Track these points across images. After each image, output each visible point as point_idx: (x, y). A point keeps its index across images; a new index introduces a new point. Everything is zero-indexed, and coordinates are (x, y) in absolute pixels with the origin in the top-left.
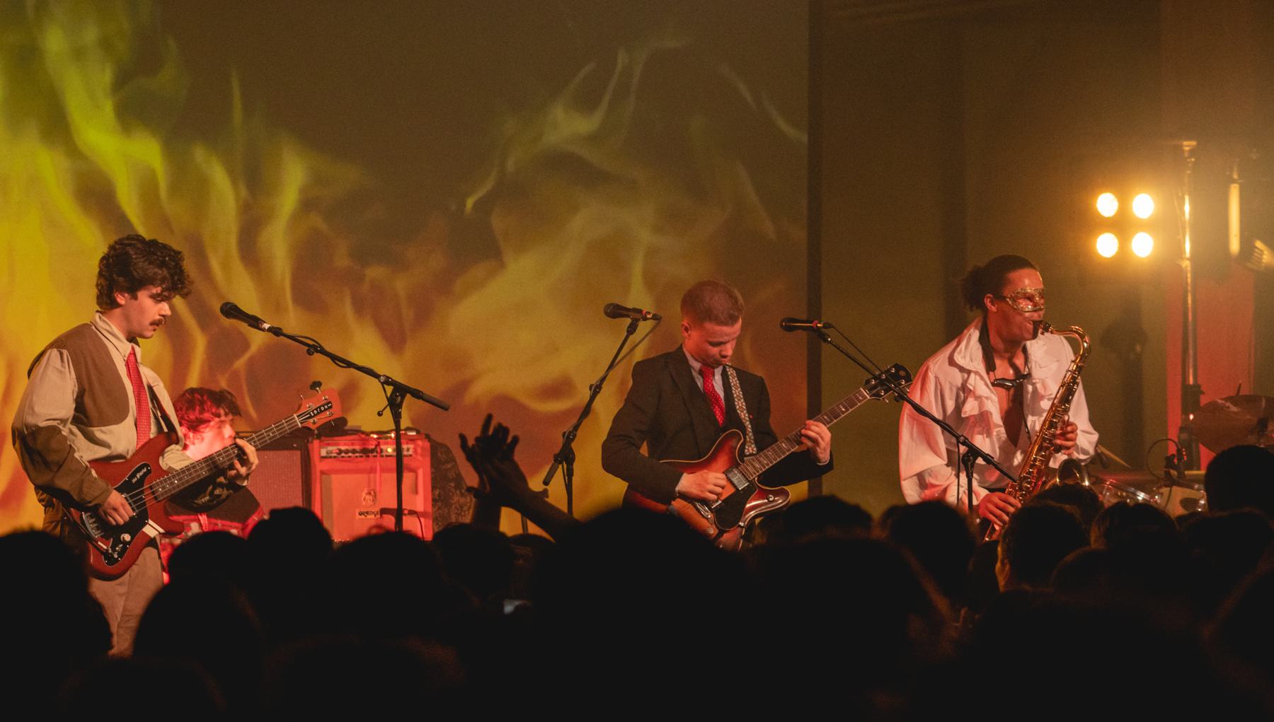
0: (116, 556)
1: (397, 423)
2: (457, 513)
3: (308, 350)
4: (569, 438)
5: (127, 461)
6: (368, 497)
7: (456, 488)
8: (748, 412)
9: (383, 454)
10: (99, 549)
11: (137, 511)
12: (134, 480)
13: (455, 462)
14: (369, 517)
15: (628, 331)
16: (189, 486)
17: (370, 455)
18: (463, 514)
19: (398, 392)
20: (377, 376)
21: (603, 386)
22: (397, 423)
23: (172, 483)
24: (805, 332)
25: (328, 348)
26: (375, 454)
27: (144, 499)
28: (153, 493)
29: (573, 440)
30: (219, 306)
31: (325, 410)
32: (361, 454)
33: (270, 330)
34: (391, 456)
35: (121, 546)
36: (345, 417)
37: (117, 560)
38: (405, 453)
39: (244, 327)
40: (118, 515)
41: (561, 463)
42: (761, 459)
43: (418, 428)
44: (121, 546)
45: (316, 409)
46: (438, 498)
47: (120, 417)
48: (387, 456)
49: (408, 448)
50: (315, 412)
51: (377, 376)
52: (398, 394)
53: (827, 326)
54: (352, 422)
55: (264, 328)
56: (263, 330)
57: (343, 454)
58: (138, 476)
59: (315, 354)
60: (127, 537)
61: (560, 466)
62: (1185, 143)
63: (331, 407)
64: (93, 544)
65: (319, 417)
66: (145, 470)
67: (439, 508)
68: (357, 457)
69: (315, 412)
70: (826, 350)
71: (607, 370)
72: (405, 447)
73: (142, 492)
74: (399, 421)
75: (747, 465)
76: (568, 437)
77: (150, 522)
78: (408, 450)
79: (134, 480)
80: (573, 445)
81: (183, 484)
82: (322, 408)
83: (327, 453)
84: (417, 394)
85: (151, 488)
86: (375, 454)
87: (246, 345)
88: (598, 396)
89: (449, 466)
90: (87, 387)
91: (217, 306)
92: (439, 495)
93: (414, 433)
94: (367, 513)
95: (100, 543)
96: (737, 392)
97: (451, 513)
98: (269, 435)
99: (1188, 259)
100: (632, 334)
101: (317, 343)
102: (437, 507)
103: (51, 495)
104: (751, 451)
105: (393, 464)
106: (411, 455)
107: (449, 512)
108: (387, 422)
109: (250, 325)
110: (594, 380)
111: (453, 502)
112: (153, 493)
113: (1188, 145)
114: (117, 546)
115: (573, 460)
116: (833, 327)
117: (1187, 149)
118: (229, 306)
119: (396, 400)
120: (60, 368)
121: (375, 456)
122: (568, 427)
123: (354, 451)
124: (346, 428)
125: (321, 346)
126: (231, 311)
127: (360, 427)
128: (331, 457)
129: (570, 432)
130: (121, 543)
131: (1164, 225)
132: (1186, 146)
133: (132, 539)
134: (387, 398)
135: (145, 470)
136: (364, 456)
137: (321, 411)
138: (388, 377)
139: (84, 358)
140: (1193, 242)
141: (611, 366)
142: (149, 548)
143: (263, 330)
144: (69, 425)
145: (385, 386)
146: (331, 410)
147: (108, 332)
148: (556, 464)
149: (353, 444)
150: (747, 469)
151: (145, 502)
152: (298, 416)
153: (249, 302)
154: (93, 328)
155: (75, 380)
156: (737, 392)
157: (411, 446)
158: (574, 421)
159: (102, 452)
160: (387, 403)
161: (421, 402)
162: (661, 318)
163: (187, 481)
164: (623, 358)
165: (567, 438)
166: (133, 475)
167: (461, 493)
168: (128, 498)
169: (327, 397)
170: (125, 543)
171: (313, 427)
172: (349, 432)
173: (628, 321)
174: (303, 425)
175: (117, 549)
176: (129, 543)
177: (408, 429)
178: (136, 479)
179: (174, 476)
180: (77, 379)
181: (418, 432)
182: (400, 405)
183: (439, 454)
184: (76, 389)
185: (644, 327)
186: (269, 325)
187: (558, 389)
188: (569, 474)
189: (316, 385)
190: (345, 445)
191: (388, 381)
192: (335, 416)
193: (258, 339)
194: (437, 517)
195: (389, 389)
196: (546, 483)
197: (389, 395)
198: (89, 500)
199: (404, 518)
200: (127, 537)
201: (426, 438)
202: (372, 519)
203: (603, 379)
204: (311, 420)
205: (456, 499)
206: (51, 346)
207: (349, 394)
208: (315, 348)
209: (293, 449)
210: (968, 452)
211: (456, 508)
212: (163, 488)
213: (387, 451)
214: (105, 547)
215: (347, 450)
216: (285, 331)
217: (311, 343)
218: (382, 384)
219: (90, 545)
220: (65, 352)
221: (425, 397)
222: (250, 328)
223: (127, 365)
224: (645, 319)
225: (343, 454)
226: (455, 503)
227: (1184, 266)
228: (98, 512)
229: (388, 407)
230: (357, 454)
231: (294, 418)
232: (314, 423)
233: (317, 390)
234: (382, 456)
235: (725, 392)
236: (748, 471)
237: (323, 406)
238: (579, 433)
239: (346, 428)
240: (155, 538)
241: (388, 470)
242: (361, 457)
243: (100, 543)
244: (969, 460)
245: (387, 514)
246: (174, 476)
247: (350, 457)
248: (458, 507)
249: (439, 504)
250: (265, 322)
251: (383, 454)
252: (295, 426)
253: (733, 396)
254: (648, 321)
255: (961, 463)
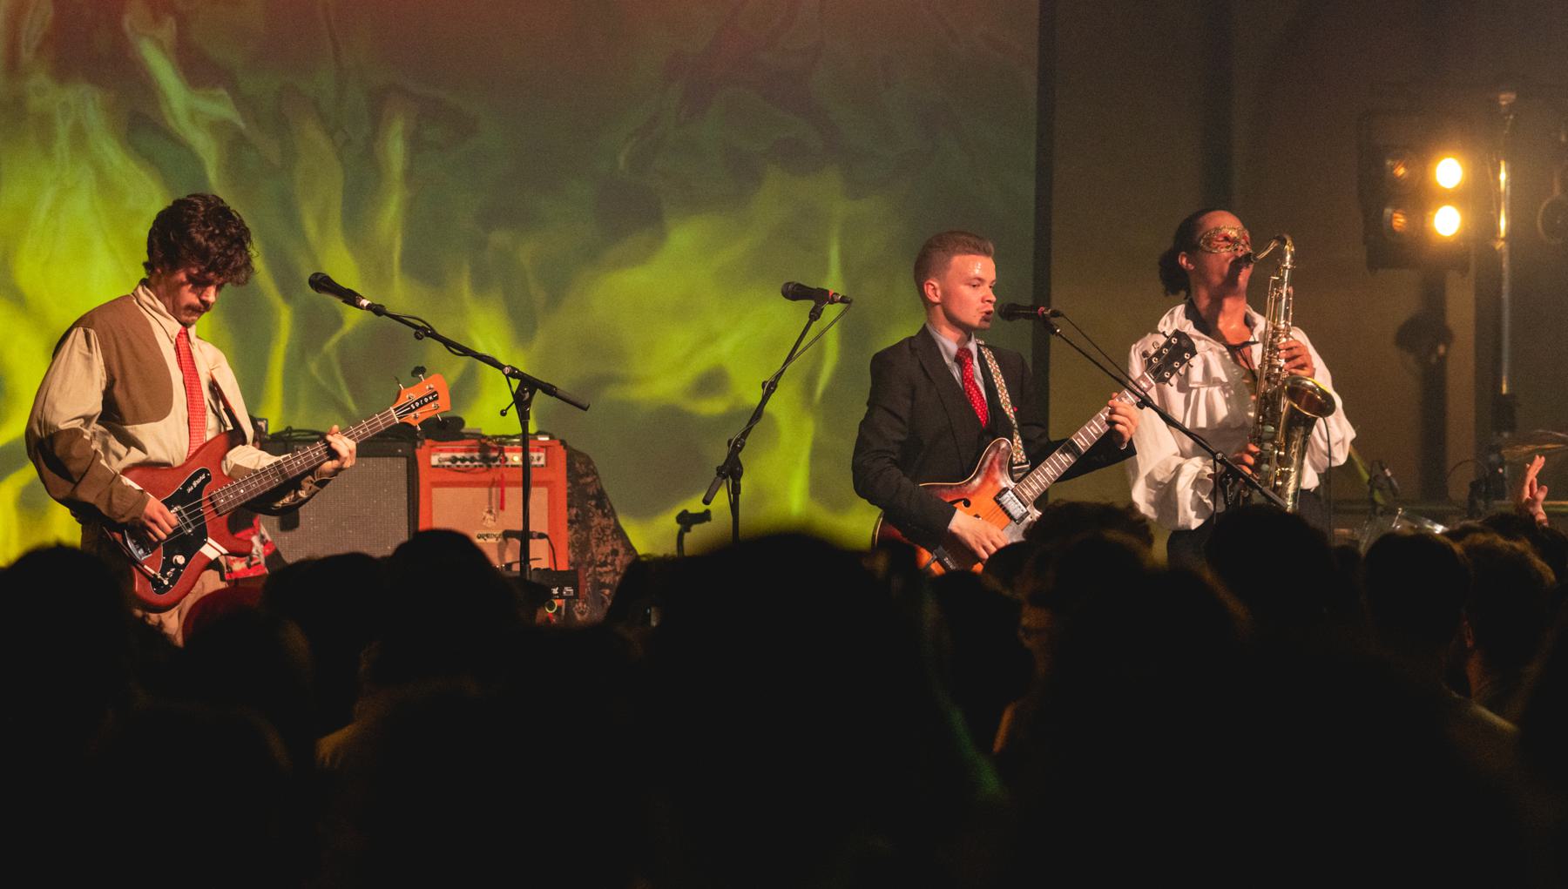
0: (166, 582)
1: (524, 425)
2: (598, 539)
3: (416, 334)
4: (736, 448)
5: (1165, 485)
6: (488, 516)
7: (597, 506)
8: (1013, 406)
9: (509, 463)
10: (144, 573)
11: (193, 527)
12: (190, 490)
13: (596, 474)
14: (489, 540)
15: (810, 316)
16: (258, 496)
17: (492, 464)
18: (605, 538)
19: (526, 386)
20: (499, 366)
21: (779, 383)
22: (524, 425)
23: (237, 493)
24: (1031, 322)
25: (440, 332)
26: (498, 463)
27: (202, 512)
28: (213, 505)
29: (741, 449)
30: (309, 275)
31: (430, 401)
32: (481, 463)
33: (369, 307)
34: (517, 466)
35: (173, 570)
36: (462, 416)
37: (167, 588)
38: (535, 463)
39: (338, 302)
40: (159, 527)
41: (725, 477)
42: (1038, 477)
43: (550, 431)
44: (173, 570)
45: (418, 401)
46: (574, 518)
47: (161, 410)
48: (512, 466)
49: (538, 458)
50: (417, 404)
51: (499, 366)
52: (526, 389)
53: (1055, 314)
54: (470, 425)
55: (363, 306)
56: (361, 307)
57: (459, 463)
58: (195, 484)
59: (425, 338)
60: (180, 559)
61: (725, 481)
62: (1503, 96)
63: (437, 398)
64: (137, 568)
65: (422, 410)
66: (203, 477)
67: (576, 532)
68: (476, 466)
69: (417, 404)
70: (1055, 342)
71: (785, 364)
72: (534, 455)
73: (200, 504)
74: (527, 422)
75: (1024, 487)
76: (735, 446)
77: (210, 540)
78: (539, 459)
79: (190, 490)
80: (741, 456)
81: (251, 493)
82: (426, 400)
83: (439, 461)
84: (549, 390)
85: (211, 499)
86: (498, 463)
87: (339, 321)
88: (773, 396)
89: (589, 480)
90: (118, 377)
91: (307, 273)
92: (577, 515)
93: (547, 439)
94: (487, 536)
95: (146, 567)
96: (999, 381)
97: (591, 538)
98: (358, 433)
99: (1503, 239)
100: (815, 320)
101: (427, 325)
102: (573, 530)
103: (81, 511)
104: (1019, 460)
105: (519, 476)
106: (542, 466)
107: (588, 535)
108: (512, 425)
109: (345, 302)
110: (768, 376)
111: (592, 524)
112: (213, 505)
113: (1506, 99)
114: (169, 570)
115: (740, 474)
116: (1062, 315)
117: (1504, 103)
118: (320, 277)
119: (524, 397)
120: (87, 353)
121: (498, 466)
122: (735, 434)
123: (472, 460)
124: (463, 431)
125: (432, 329)
126: (322, 283)
127: (480, 429)
128: (443, 466)
129: (738, 440)
130: (173, 566)
131: (1476, 197)
132: (1503, 100)
133: (187, 561)
134: (512, 393)
135: (203, 477)
136: (485, 466)
137: (425, 403)
138: (514, 369)
139: (115, 339)
140: (1512, 217)
141: (790, 359)
142: (211, 571)
143: (361, 307)
144: (94, 425)
145: (510, 379)
146: (436, 402)
147: (150, 306)
148: (720, 478)
149: (471, 451)
150: (1023, 492)
151: (203, 516)
152: (395, 410)
153: (344, 272)
154: (135, 301)
155: (103, 368)
156: (999, 381)
157: (542, 454)
158: (744, 426)
159: (136, 456)
160: (512, 400)
161: (553, 399)
162: (851, 300)
163: (256, 490)
164: (804, 350)
165: (733, 446)
166: (189, 483)
167: (603, 512)
168: (182, 511)
169: (432, 386)
170: (178, 566)
171: (415, 423)
172: (467, 436)
173: (811, 304)
174: (403, 420)
175: (168, 573)
176: (184, 566)
177: (540, 433)
178: (192, 488)
179: (239, 485)
180: (105, 366)
181: (552, 437)
182: (528, 403)
183: (577, 465)
184: (105, 378)
185: (831, 312)
186: (368, 302)
187: (712, 382)
188: (735, 491)
189: (420, 370)
190: (461, 451)
191: (514, 374)
192: (441, 410)
193: (353, 317)
194: (573, 543)
195: (515, 383)
196: (706, 502)
197: (514, 390)
198: (120, 512)
199: (531, 541)
200: (180, 559)
201: (561, 444)
202: (492, 544)
203: (779, 375)
204: (412, 415)
205: (596, 521)
206: (76, 324)
207: (465, 389)
208: (425, 332)
209: (394, 455)
210: (1226, 472)
211: (596, 531)
212: (227, 498)
213: (513, 460)
214: (153, 572)
215: (464, 457)
216: (388, 310)
217: (421, 324)
218: (507, 376)
219: (135, 570)
220: (92, 332)
221: (559, 392)
222: (343, 304)
223: (177, 348)
224: (832, 302)
225: (459, 463)
226: (595, 526)
227: (1498, 247)
228: (140, 530)
229: (514, 406)
230: (476, 463)
231: (390, 412)
232: (416, 417)
233: (420, 378)
234: (507, 466)
235: (986, 388)
236: (1025, 494)
237: (427, 397)
238: (748, 441)
239: (463, 431)
240: (217, 559)
241: (514, 484)
242: (480, 466)
243: (146, 567)
244: (1228, 482)
245: (512, 537)
246: (239, 485)
247: (467, 466)
248: (599, 530)
249: (576, 526)
250: (363, 298)
251: (508, 463)
252: (390, 422)
253: (995, 386)
254: (835, 305)
255: (1218, 487)
